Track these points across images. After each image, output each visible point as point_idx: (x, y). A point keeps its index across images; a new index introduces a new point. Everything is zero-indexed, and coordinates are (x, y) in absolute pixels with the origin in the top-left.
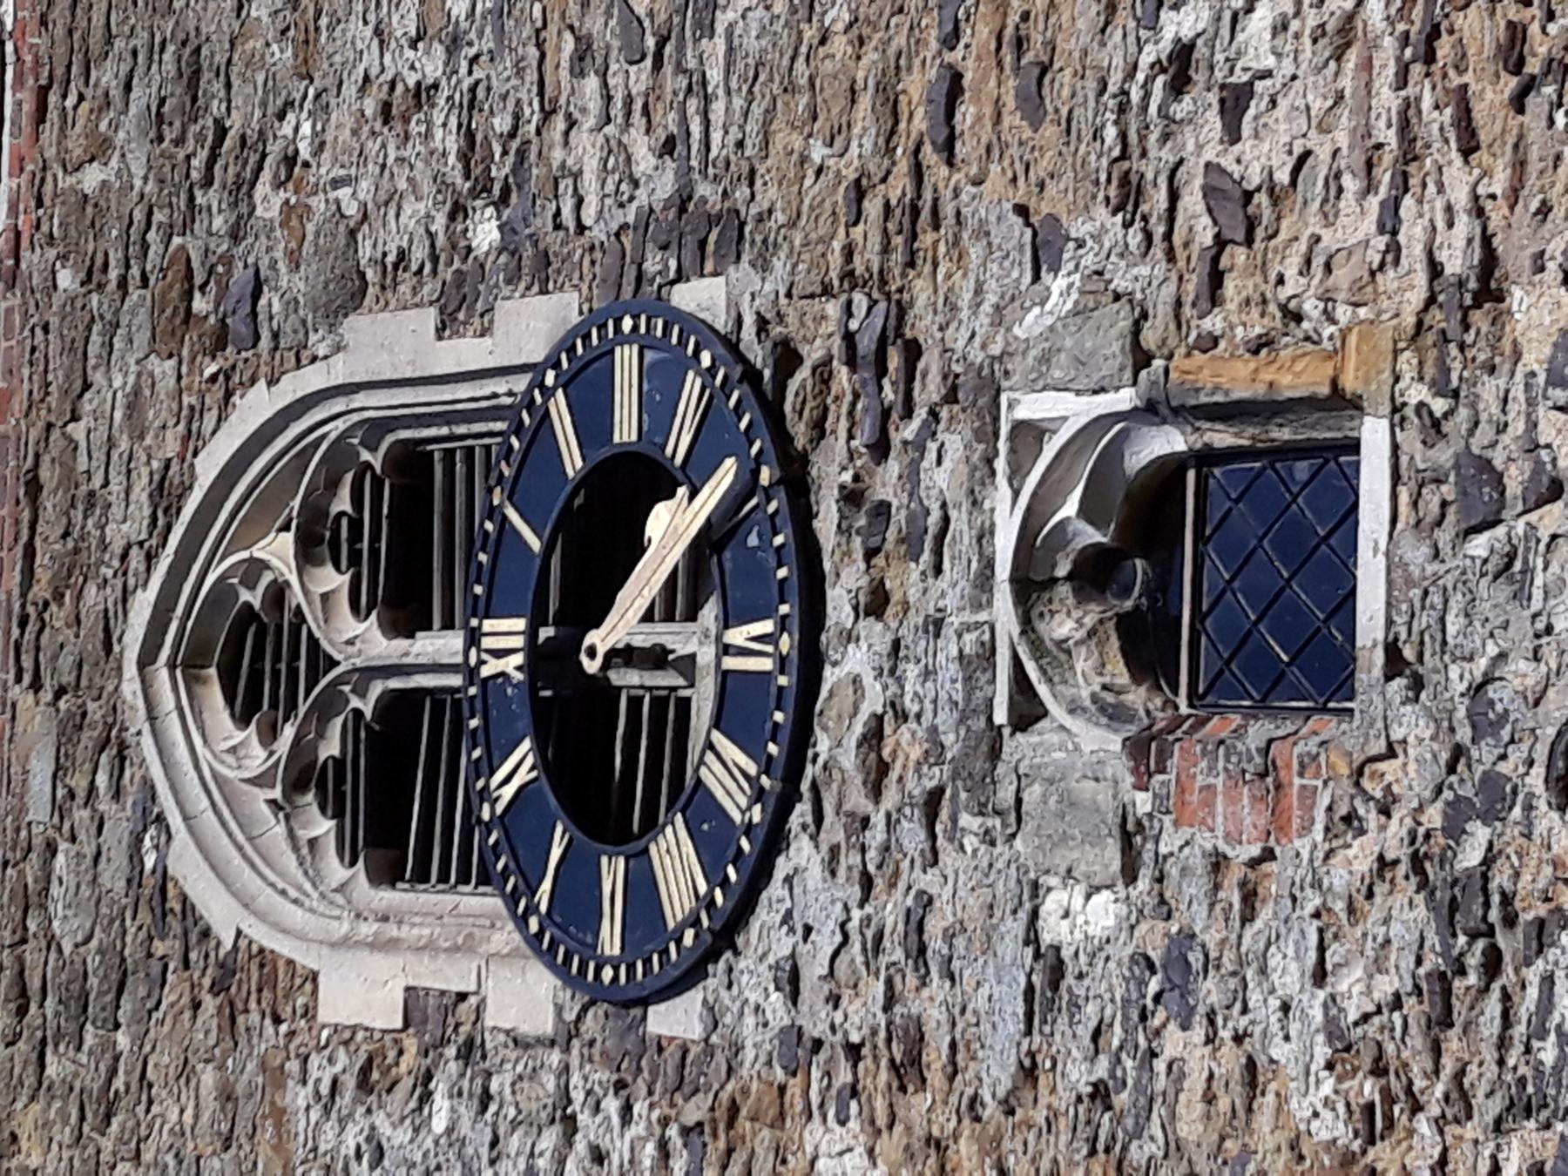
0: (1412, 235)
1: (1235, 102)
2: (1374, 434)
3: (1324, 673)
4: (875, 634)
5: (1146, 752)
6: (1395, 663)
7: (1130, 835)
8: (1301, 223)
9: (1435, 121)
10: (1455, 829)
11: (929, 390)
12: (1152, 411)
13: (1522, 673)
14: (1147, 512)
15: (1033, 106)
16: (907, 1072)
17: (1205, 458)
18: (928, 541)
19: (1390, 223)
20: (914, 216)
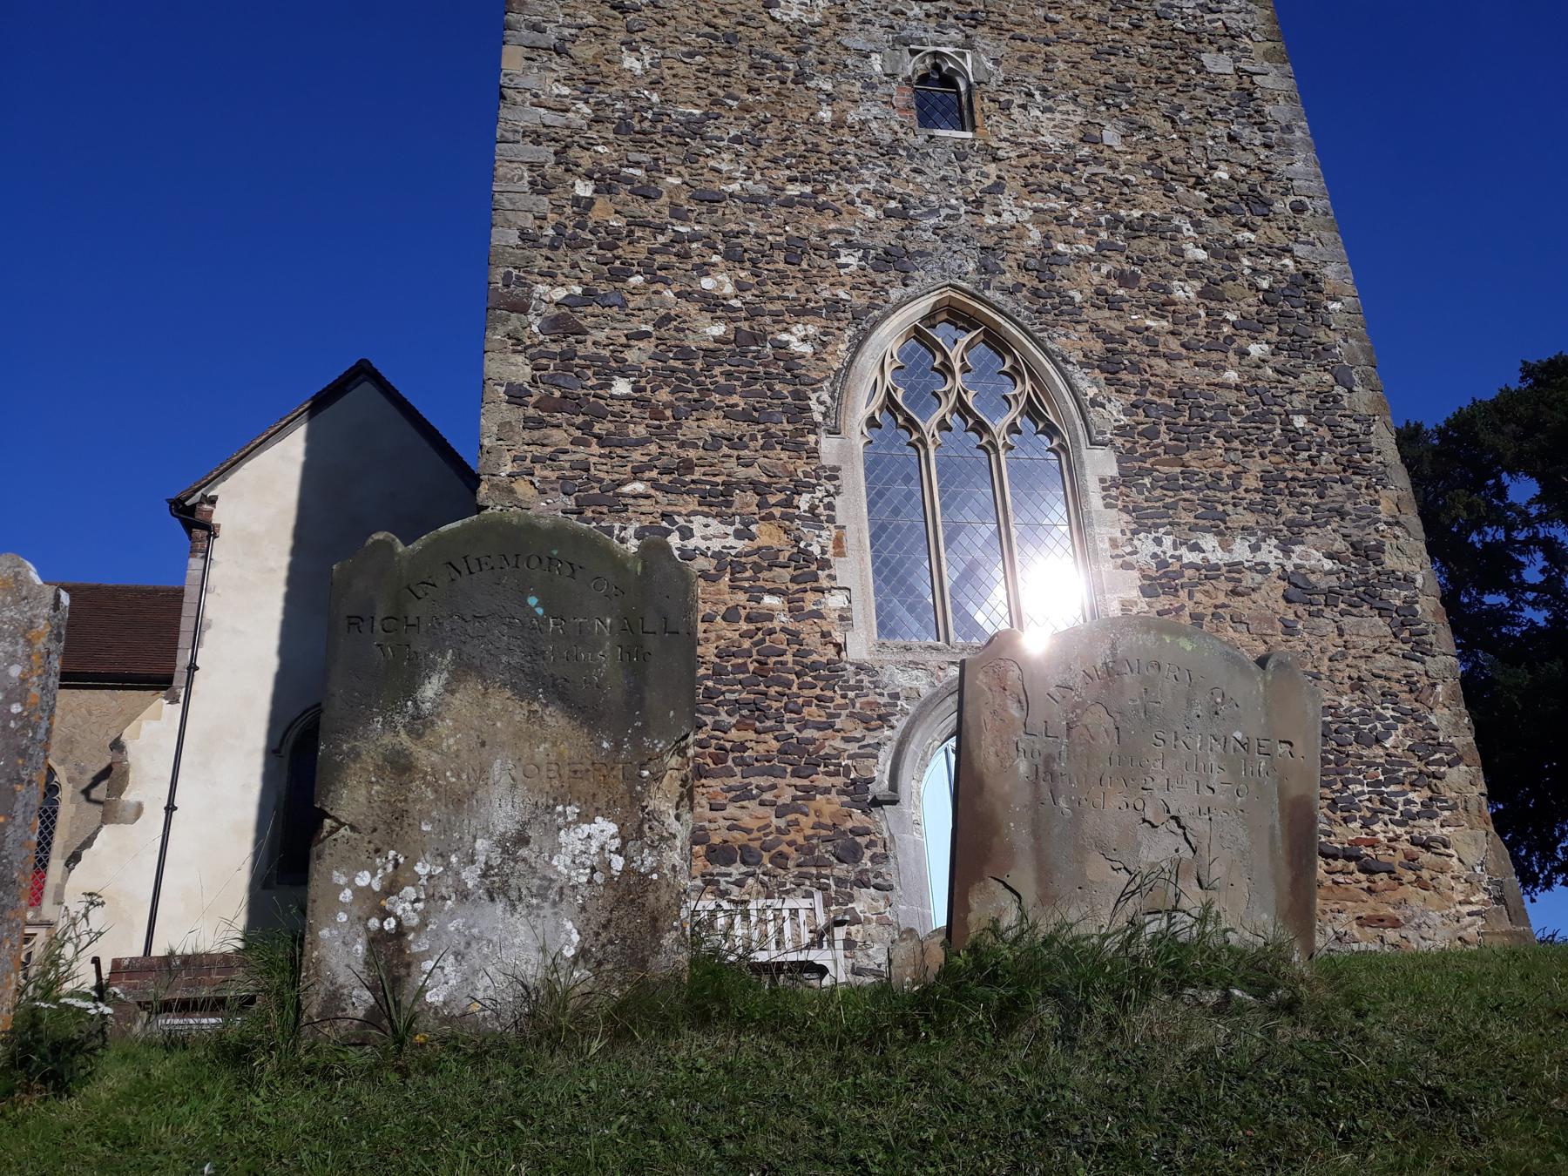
0: (1004, 144)
1: (1024, 107)
2: (969, 135)
3: (926, 120)
4: (922, 16)
5: (908, 80)
6: (931, 137)
7: (893, 76)
8: (1003, 119)
9: (1023, 150)
10: (905, 149)
11: (970, 31)
12: (969, 85)
13: (932, 164)
14: (948, 80)
15: (1021, 59)
16: (841, 18)
17: (958, 93)
18: (941, 29)
19: (1005, 140)
20: (999, 29)
